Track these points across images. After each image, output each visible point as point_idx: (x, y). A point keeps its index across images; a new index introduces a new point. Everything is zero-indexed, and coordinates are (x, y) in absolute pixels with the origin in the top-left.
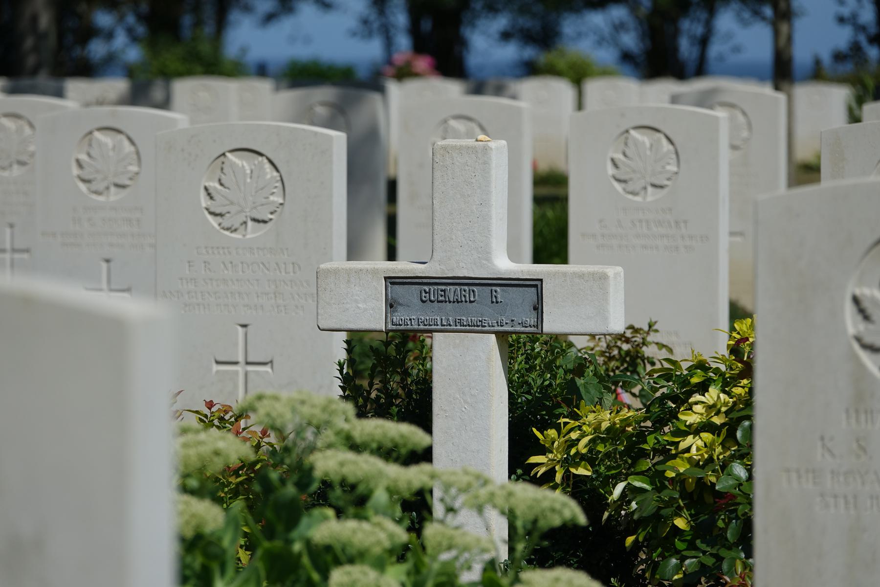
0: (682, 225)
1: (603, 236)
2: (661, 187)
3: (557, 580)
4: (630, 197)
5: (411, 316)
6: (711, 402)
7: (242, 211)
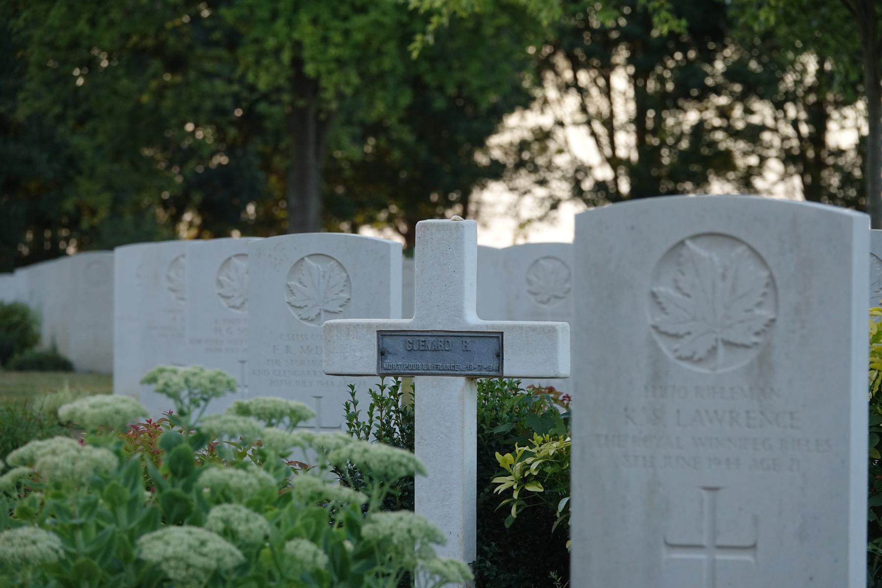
3: (401, 519)
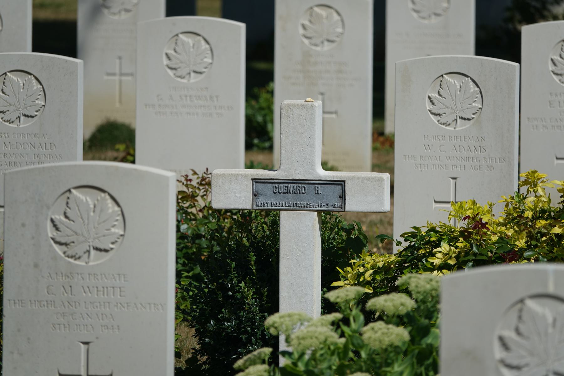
0: (215, 99)
1: (160, 106)
2: (201, 73)
4: (179, 79)
5: (268, 201)
6: (446, 252)
7: (18, 110)
